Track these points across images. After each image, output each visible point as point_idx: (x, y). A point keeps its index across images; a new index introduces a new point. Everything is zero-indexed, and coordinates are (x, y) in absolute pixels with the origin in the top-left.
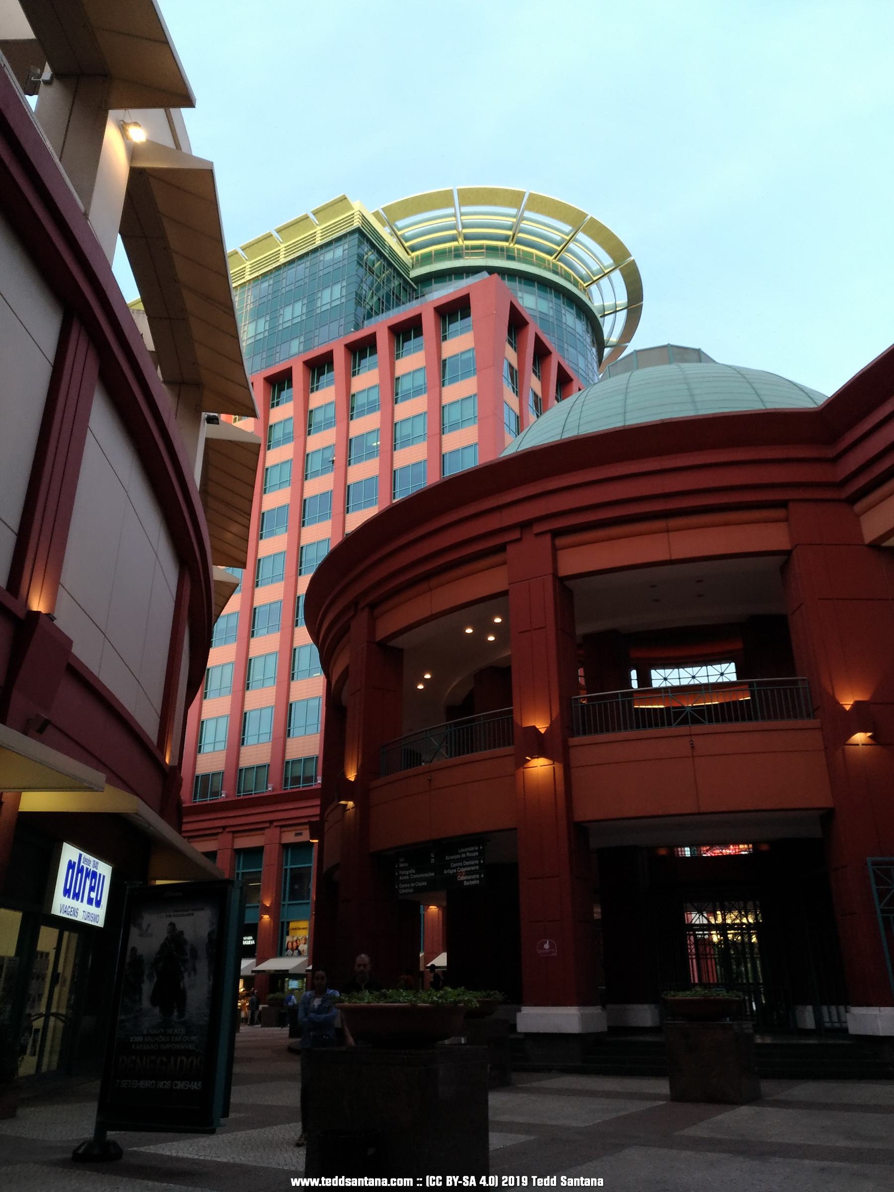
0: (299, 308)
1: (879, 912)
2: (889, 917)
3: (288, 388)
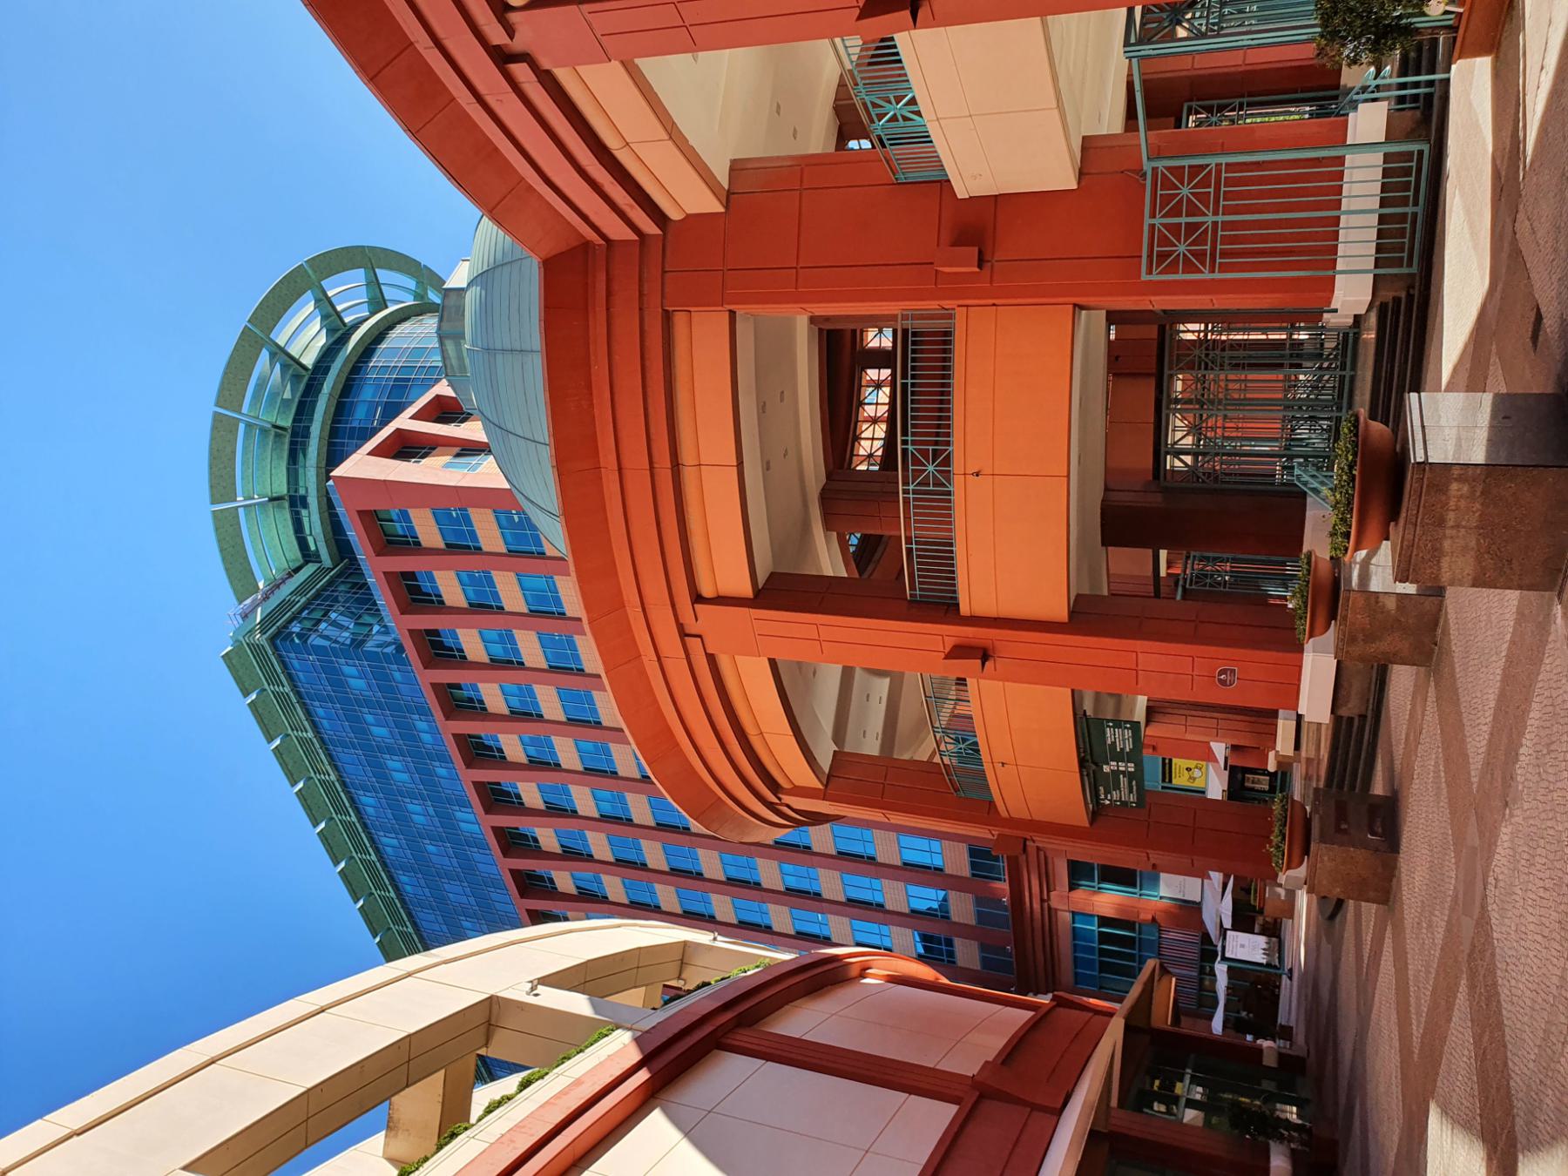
0: (394, 763)
1: (1212, 276)
2: (1226, 178)
3: (439, 636)
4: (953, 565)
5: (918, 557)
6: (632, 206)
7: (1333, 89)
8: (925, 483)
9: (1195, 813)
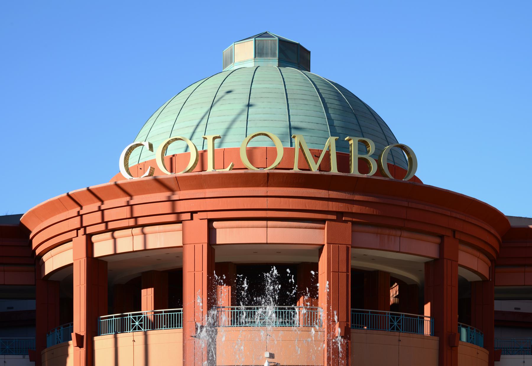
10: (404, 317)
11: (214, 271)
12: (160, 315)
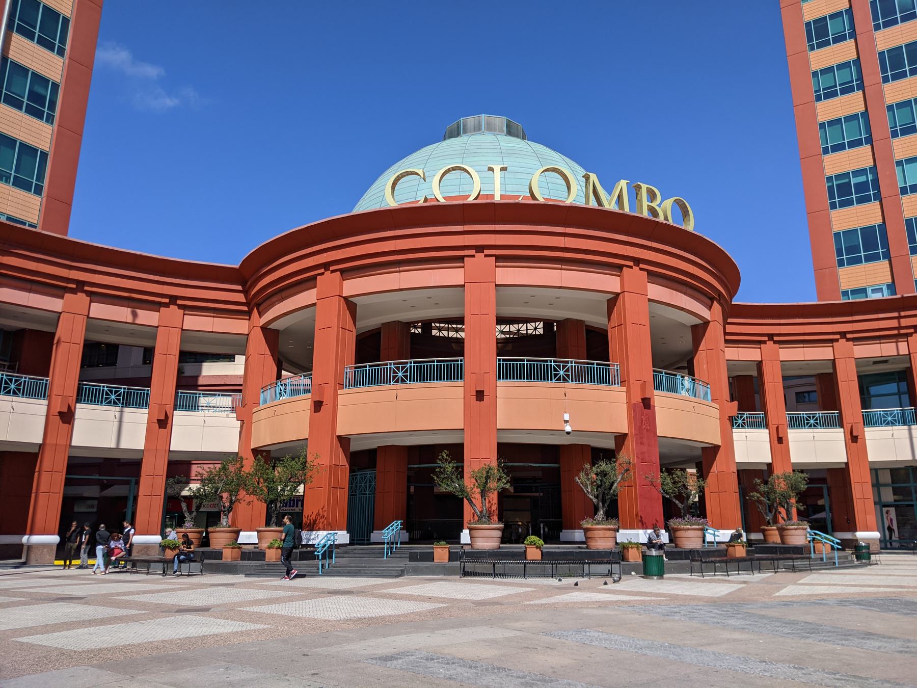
4: (444, 379)
5: (431, 365)
6: (395, 232)
7: (832, 527)
8: (555, 370)
9: (389, 492)
10: (573, 365)
11: (555, 329)
12: (384, 368)
